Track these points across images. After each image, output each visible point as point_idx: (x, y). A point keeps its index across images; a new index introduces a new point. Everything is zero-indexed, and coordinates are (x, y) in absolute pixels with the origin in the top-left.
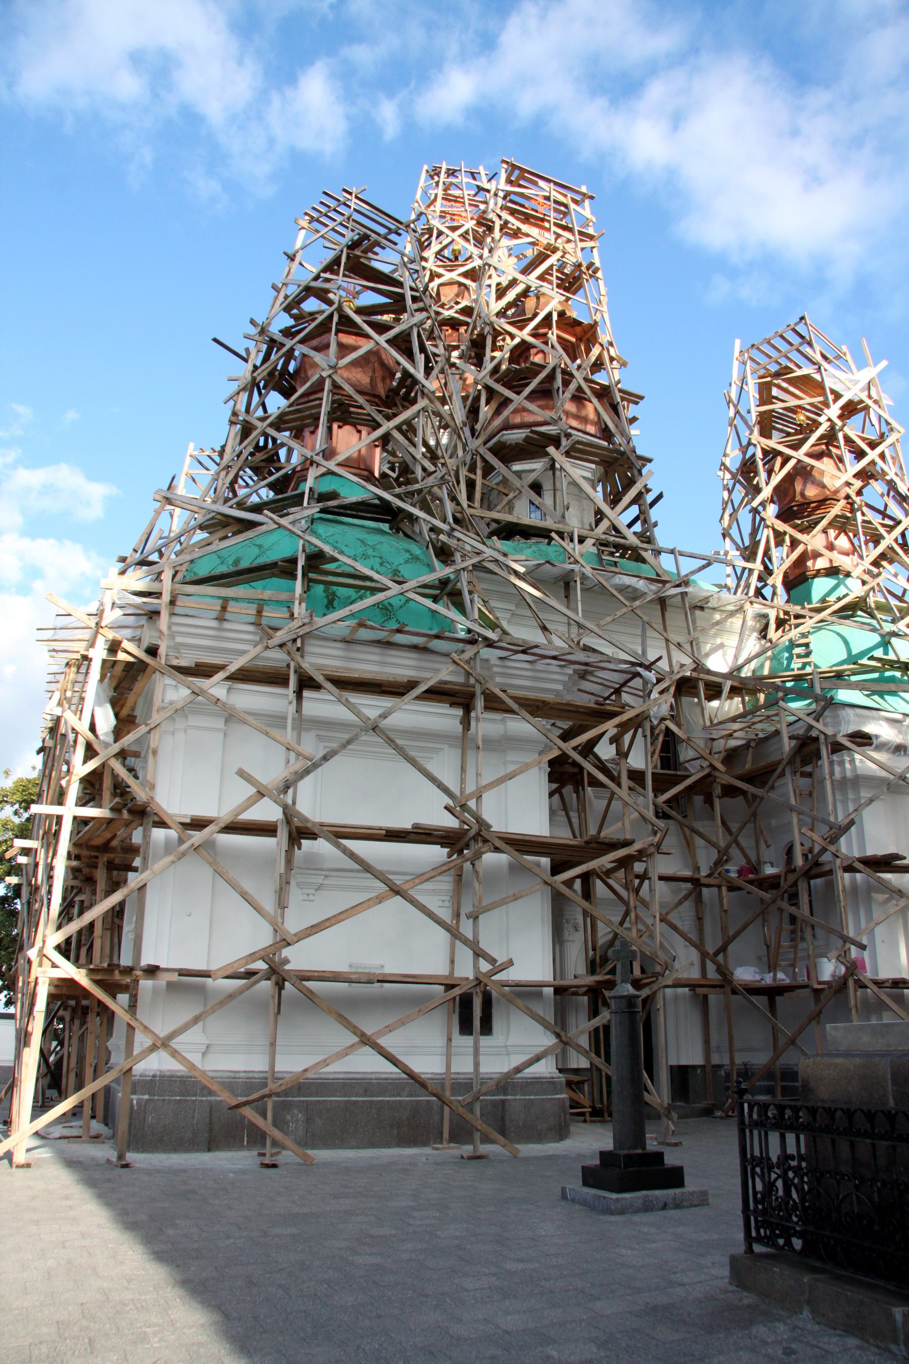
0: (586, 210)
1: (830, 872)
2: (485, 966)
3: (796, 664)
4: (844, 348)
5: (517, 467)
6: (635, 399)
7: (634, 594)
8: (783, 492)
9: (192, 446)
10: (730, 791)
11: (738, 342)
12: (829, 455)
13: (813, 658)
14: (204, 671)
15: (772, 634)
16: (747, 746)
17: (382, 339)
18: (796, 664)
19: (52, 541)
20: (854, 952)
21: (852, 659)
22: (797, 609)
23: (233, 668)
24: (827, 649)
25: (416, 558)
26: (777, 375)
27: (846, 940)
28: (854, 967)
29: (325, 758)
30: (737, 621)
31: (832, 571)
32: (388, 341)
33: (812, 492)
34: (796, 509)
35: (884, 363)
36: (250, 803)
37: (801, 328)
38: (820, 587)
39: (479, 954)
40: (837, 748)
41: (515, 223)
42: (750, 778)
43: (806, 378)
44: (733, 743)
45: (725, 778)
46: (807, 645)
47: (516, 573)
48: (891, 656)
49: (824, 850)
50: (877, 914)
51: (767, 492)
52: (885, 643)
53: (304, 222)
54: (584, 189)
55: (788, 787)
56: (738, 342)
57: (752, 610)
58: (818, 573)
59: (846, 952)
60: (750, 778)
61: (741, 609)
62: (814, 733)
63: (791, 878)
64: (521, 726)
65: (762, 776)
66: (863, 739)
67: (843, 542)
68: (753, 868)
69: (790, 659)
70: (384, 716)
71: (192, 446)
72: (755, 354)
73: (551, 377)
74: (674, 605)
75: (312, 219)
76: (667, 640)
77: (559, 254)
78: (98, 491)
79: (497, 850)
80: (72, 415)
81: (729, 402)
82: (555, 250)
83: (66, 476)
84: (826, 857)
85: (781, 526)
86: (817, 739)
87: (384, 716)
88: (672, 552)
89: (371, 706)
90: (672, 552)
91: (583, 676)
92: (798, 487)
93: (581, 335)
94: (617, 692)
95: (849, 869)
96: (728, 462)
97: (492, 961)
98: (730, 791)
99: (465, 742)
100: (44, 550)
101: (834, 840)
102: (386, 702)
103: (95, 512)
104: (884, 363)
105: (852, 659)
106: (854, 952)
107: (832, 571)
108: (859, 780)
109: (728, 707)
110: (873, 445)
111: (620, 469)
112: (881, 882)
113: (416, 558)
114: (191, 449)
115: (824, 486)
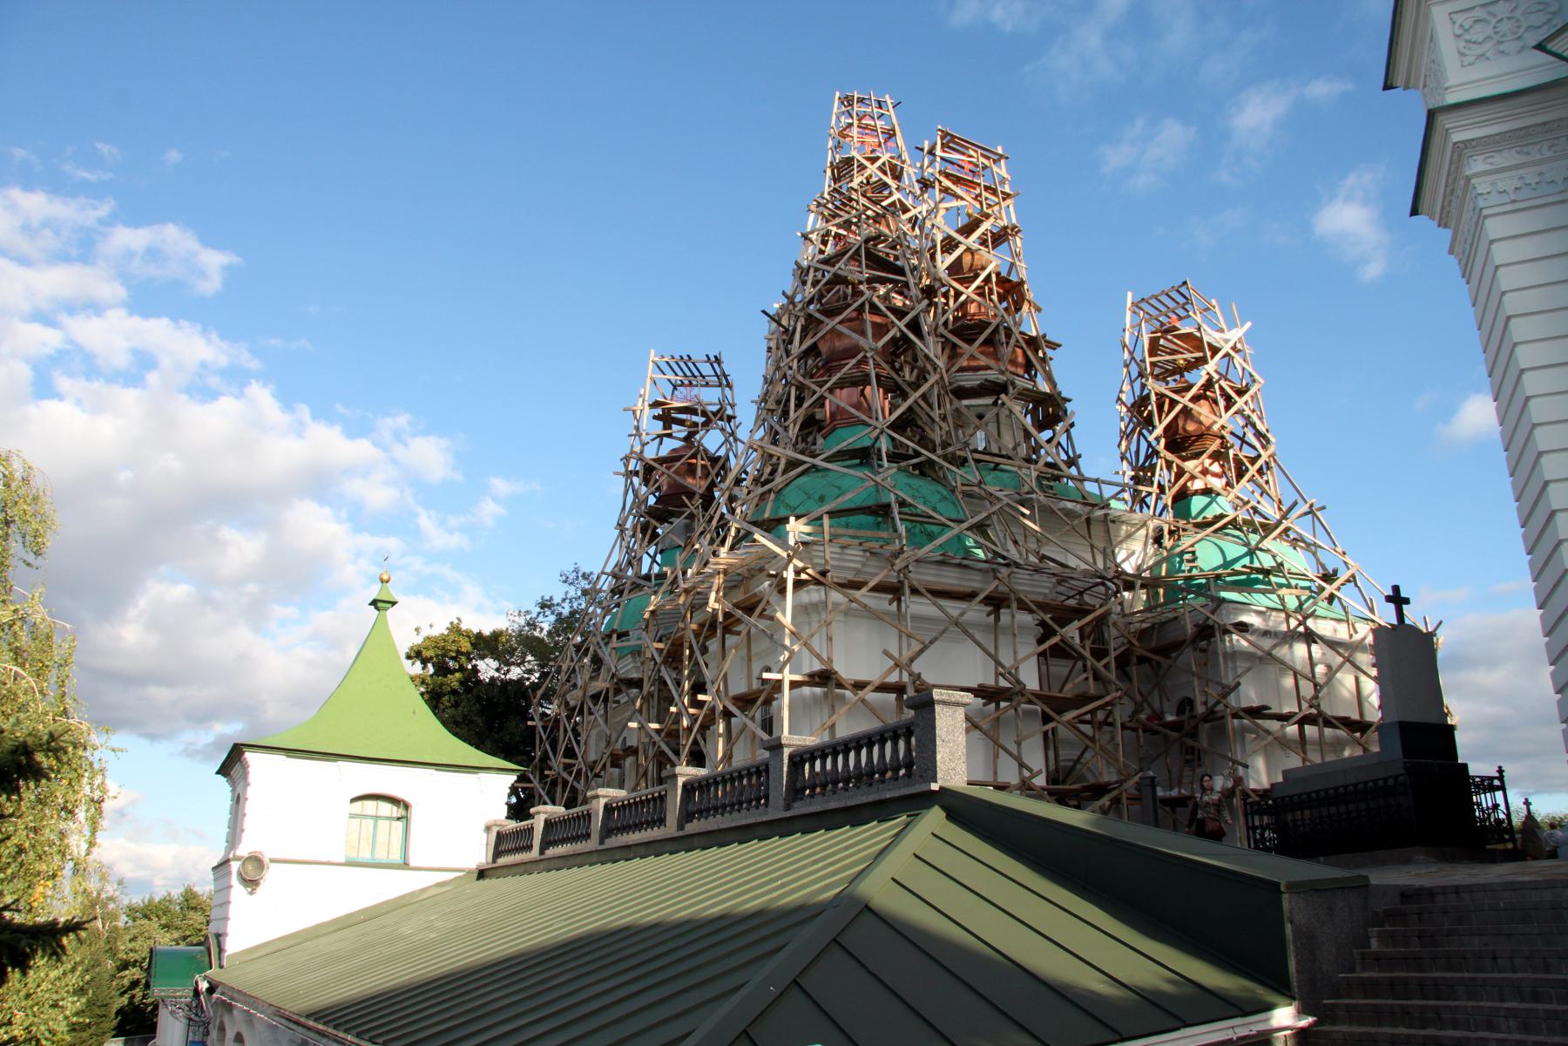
0: (1001, 170)
1: (1223, 717)
2: (1026, 774)
3: (1185, 566)
4: (1214, 302)
5: (966, 402)
6: (1054, 346)
7: (1069, 514)
8: (1170, 430)
9: (653, 352)
10: (1142, 660)
11: (1129, 295)
12: (1206, 398)
13: (1199, 563)
14: (857, 585)
15: (1167, 542)
16: (1152, 627)
17: (901, 324)
18: (1185, 566)
19: (165, 321)
20: (1241, 771)
21: (1227, 564)
22: (1182, 523)
23: (872, 584)
24: (1208, 555)
25: (945, 498)
26: (1167, 331)
27: (1235, 762)
28: (1239, 781)
29: (931, 643)
30: (1143, 532)
31: (1207, 492)
32: (907, 326)
33: (1191, 427)
34: (1180, 443)
35: (1249, 324)
36: (891, 671)
37: (1183, 290)
38: (1197, 503)
39: (1022, 765)
40: (1226, 632)
41: (947, 183)
42: (1156, 651)
43: (1189, 335)
44: (1145, 625)
45: (1139, 651)
46: (1193, 553)
47: (1024, 515)
48: (1256, 564)
49: (1218, 702)
50: (1249, 748)
51: (1159, 430)
52: (1251, 553)
53: (813, 207)
54: (1000, 150)
55: (1188, 657)
56: (1129, 295)
57: (1152, 525)
58: (1196, 493)
59: (1235, 770)
60: (1156, 651)
61: (1144, 524)
62: (1210, 622)
63: (1193, 723)
64: (1025, 618)
65: (1170, 649)
66: (1243, 628)
67: (1216, 468)
68: (1158, 716)
69: (1181, 562)
70: (962, 614)
71: (653, 352)
72: (1144, 305)
73: (996, 330)
74: (1095, 522)
75: (819, 205)
76: (1092, 547)
77: (992, 220)
78: (214, 260)
79: (1030, 702)
80: (174, 156)
81: (1125, 346)
82: (988, 216)
83: (172, 235)
84: (1220, 707)
85: (1170, 457)
86: (1212, 627)
87: (962, 614)
88: (1097, 481)
89: (954, 608)
90: (1097, 481)
91: (1059, 583)
92: (1181, 423)
93: (1012, 291)
94: (1081, 593)
95: (1235, 716)
96: (1123, 397)
97: (1030, 770)
98: (1142, 660)
99: (996, 628)
100: (158, 332)
101: (1225, 696)
102: (963, 605)
103: (211, 285)
104: (1249, 324)
105: (1227, 564)
106: (1241, 771)
107: (1207, 492)
108: (1235, 655)
109: (1136, 600)
110: (1241, 393)
111: (1050, 410)
112: (1257, 725)
113: (945, 498)
114: (653, 355)
115: (1201, 423)
